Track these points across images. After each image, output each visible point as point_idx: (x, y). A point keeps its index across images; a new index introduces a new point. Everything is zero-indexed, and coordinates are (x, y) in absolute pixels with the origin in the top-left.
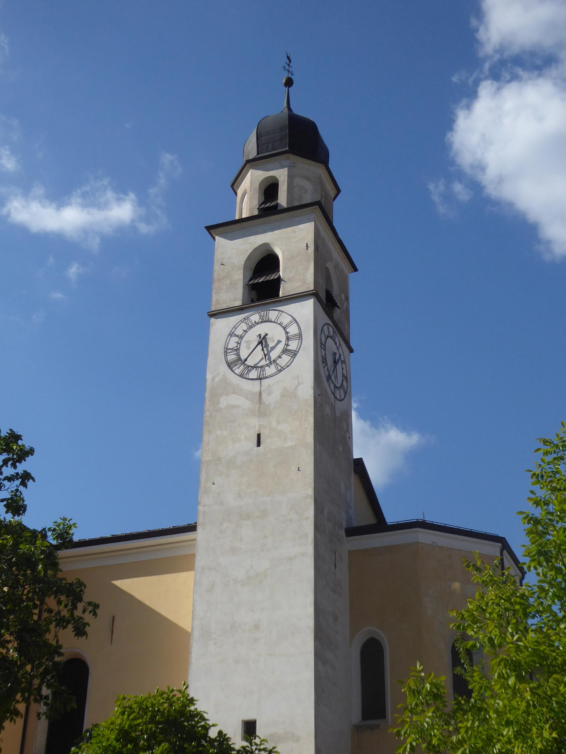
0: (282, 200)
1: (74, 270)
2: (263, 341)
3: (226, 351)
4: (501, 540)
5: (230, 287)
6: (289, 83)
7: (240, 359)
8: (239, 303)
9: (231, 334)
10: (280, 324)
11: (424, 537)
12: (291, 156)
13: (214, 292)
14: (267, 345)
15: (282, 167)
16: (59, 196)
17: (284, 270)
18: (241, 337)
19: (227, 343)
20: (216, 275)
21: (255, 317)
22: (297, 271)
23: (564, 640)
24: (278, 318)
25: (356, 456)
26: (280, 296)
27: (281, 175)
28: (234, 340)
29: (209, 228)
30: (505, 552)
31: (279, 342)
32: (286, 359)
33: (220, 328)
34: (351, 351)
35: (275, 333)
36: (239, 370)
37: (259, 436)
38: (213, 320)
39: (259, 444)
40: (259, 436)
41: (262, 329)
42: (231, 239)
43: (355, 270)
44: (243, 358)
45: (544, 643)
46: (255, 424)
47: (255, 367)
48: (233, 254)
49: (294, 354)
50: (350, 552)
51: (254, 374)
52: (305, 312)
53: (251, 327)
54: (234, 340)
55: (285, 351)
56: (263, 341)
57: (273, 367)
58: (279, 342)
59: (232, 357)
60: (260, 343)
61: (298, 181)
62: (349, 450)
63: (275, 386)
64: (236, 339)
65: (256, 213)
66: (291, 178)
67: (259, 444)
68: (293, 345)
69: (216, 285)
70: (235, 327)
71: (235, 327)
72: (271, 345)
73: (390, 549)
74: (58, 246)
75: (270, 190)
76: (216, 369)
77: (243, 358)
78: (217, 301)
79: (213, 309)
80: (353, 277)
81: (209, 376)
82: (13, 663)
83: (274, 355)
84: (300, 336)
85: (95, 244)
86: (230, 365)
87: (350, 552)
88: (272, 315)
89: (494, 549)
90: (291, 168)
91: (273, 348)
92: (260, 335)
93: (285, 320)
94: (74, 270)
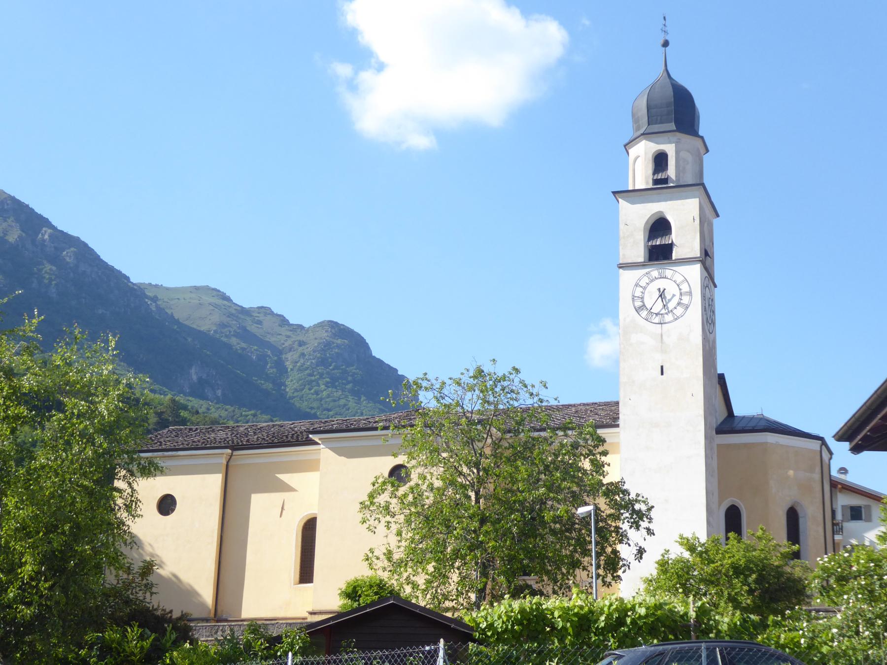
0: (671, 171)
2: (662, 295)
3: (634, 298)
4: (821, 439)
5: (635, 247)
6: (666, 44)
7: (644, 305)
8: (641, 259)
9: (637, 285)
10: (675, 282)
12: (678, 134)
13: (621, 248)
14: (665, 298)
15: (670, 143)
17: (676, 236)
18: (645, 288)
19: (634, 292)
20: (621, 234)
21: (655, 273)
22: (685, 240)
23: (615, 663)
24: (672, 276)
25: (719, 372)
26: (674, 257)
27: (670, 149)
28: (639, 290)
29: (614, 193)
30: (823, 447)
31: (674, 295)
32: (679, 311)
33: (628, 278)
34: (715, 286)
36: (644, 313)
37: (662, 367)
38: (621, 270)
39: (662, 374)
40: (662, 367)
41: (661, 284)
43: (718, 216)
44: (649, 307)
45: (126, 500)
46: (658, 359)
48: (635, 217)
49: (687, 307)
50: (718, 445)
52: (694, 272)
53: (652, 281)
54: (639, 290)
55: (679, 304)
56: (662, 295)
57: (670, 315)
58: (674, 295)
59: (638, 304)
60: (661, 296)
61: (683, 154)
62: (716, 369)
63: (673, 330)
64: (641, 289)
66: (677, 152)
67: (662, 374)
68: (686, 300)
69: (622, 242)
70: (640, 280)
71: (640, 280)
72: (668, 297)
73: (746, 446)
75: (660, 161)
76: (626, 308)
77: (649, 307)
78: (624, 255)
79: (621, 262)
80: (716, 222)
83: (671, 306)
84: (690, 293)
86: (638, 310)
87: (718, 445)
88: (668, 273)
89: (815, 445)
90: (677, 143)
91: (670, 300)
92: (659, 290)
93: (679, 279)
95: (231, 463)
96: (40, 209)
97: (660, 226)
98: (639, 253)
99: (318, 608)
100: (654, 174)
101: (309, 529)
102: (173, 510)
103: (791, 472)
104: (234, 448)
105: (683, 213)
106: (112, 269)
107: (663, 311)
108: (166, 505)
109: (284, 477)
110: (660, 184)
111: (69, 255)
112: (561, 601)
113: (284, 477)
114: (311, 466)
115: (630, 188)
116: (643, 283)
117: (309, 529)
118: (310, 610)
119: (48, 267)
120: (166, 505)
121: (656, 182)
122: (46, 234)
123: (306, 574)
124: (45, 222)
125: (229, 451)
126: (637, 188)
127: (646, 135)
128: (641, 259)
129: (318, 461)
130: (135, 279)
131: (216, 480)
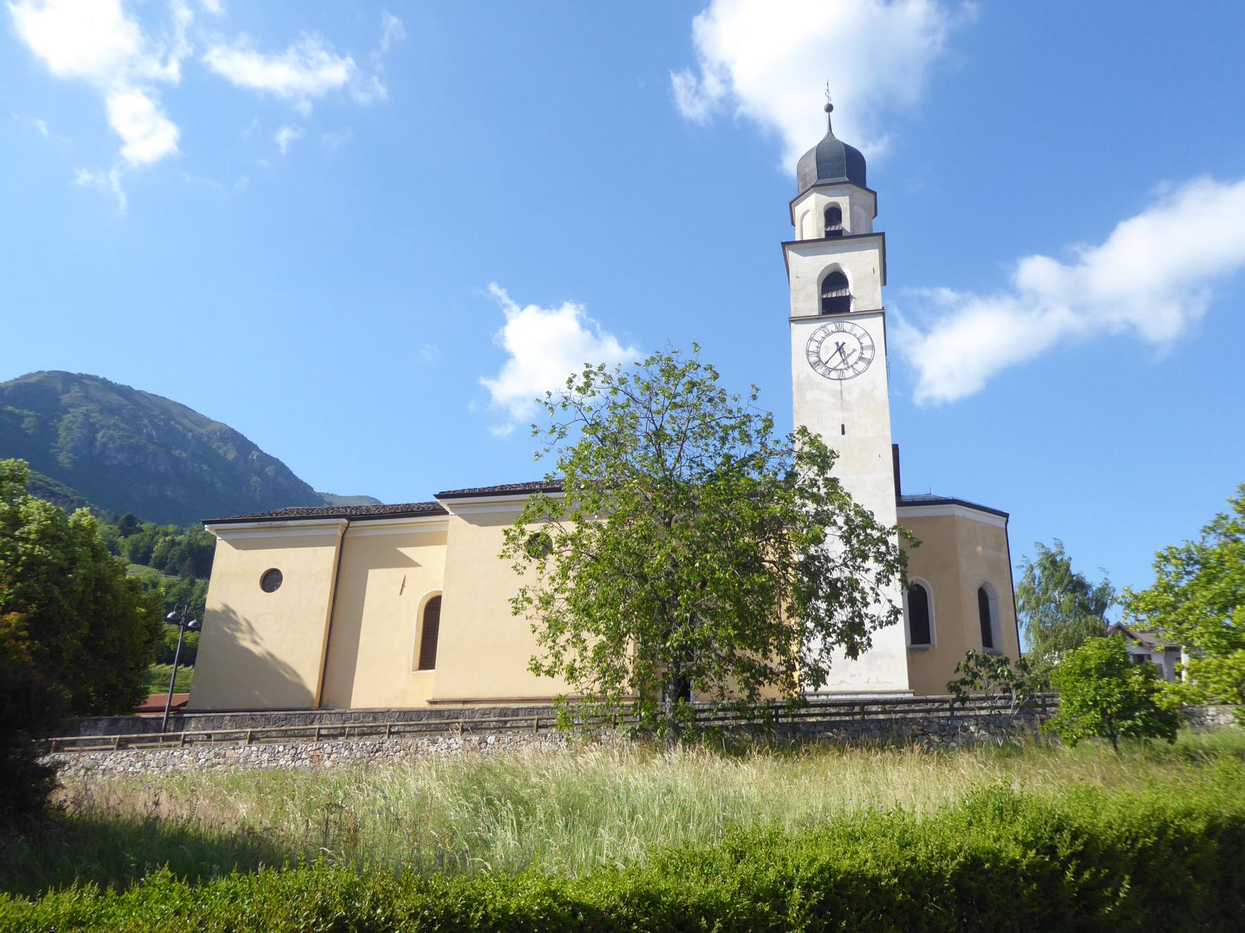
0: (846, 224)
1: (284, 136)
2: (840, 349)
3: (808, 353)
5: (807, 299)
7: (820, 360)
8: (816, 313)
9: (811, 339)
11: (958, 511)
16: (272, 43)
17: (855, 288)
18: (820, 343)
21: (831, 327)
26: (852, 310)
27: (844, 202)
32: (861, 366)
33: (800, 333)
35: (851, 344)
36: (821, 369)
41: (840, 338)
42: (804, 255)
47: (834, 369)
48: (807, 271)
49: (869, 362)
51: (834, 375)
55: (861, 358)
56: (840, 349)
59: (813, 359)
63: (854, 387)
65: (823, 236)
68: (868, 354)
69: (793, 295)
70: (814, 333)
71: (814, 333)
72: (847, 352)
73: (929, 519)
74: (270, 108)
75: (832, 215)
76: (800, 367)
81: (794, 373)
82: (198, 577)
83: (851, 360)
84: (873, 347)
85: (305, 107)
86: (813, 365)
88: (847, 326)
93: (859, 332)
94: (284, 136)
95: (347, 536)
96: (251, 437)
97: (834, 280)
98: (814, 308)
99: (439, 696)
100: (826, 226)
101: (433, 608)
102: (278, 587)
103: (979, 549)
104: (351, 518)
105: (860, 266)
106: (301, 482)
107: (842, 366)
108: (271, 580)
109: (405, 551)
110: (834, 234)
111: (270, 470)
112: (274, 757)
113: (405, 551)
114: (438, 539)
115: (798, 238)
116: (818, 337)
117: (433, 608)
118: (430, 698)
119: (255, 479)
120: (271, 580)
121: (827, 233)
122: (255, 455)
123: (427, 659)
124: (255, 447)
125: (345, 521)
126: (805, 238)
127: (817, 187)
128: (816, 313)
129: (446, 533)
130: (317, 490)
131: (330, 553)
